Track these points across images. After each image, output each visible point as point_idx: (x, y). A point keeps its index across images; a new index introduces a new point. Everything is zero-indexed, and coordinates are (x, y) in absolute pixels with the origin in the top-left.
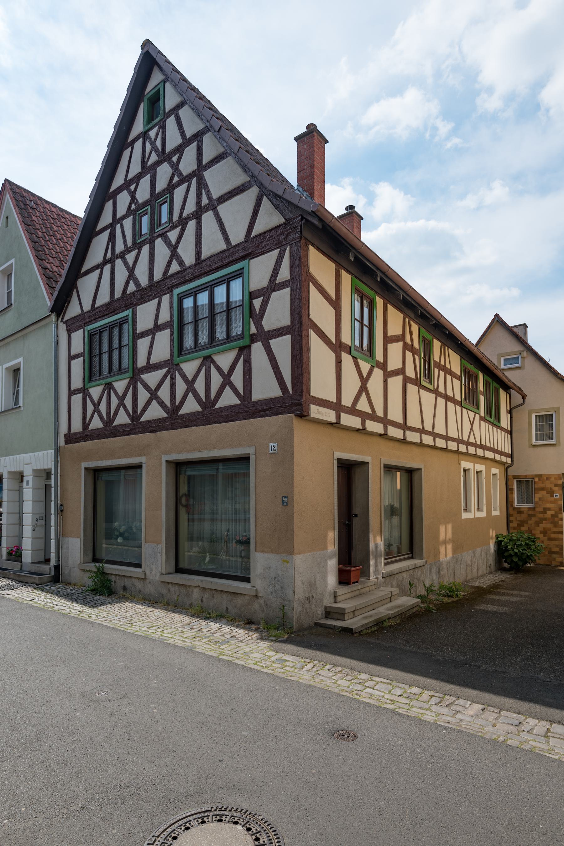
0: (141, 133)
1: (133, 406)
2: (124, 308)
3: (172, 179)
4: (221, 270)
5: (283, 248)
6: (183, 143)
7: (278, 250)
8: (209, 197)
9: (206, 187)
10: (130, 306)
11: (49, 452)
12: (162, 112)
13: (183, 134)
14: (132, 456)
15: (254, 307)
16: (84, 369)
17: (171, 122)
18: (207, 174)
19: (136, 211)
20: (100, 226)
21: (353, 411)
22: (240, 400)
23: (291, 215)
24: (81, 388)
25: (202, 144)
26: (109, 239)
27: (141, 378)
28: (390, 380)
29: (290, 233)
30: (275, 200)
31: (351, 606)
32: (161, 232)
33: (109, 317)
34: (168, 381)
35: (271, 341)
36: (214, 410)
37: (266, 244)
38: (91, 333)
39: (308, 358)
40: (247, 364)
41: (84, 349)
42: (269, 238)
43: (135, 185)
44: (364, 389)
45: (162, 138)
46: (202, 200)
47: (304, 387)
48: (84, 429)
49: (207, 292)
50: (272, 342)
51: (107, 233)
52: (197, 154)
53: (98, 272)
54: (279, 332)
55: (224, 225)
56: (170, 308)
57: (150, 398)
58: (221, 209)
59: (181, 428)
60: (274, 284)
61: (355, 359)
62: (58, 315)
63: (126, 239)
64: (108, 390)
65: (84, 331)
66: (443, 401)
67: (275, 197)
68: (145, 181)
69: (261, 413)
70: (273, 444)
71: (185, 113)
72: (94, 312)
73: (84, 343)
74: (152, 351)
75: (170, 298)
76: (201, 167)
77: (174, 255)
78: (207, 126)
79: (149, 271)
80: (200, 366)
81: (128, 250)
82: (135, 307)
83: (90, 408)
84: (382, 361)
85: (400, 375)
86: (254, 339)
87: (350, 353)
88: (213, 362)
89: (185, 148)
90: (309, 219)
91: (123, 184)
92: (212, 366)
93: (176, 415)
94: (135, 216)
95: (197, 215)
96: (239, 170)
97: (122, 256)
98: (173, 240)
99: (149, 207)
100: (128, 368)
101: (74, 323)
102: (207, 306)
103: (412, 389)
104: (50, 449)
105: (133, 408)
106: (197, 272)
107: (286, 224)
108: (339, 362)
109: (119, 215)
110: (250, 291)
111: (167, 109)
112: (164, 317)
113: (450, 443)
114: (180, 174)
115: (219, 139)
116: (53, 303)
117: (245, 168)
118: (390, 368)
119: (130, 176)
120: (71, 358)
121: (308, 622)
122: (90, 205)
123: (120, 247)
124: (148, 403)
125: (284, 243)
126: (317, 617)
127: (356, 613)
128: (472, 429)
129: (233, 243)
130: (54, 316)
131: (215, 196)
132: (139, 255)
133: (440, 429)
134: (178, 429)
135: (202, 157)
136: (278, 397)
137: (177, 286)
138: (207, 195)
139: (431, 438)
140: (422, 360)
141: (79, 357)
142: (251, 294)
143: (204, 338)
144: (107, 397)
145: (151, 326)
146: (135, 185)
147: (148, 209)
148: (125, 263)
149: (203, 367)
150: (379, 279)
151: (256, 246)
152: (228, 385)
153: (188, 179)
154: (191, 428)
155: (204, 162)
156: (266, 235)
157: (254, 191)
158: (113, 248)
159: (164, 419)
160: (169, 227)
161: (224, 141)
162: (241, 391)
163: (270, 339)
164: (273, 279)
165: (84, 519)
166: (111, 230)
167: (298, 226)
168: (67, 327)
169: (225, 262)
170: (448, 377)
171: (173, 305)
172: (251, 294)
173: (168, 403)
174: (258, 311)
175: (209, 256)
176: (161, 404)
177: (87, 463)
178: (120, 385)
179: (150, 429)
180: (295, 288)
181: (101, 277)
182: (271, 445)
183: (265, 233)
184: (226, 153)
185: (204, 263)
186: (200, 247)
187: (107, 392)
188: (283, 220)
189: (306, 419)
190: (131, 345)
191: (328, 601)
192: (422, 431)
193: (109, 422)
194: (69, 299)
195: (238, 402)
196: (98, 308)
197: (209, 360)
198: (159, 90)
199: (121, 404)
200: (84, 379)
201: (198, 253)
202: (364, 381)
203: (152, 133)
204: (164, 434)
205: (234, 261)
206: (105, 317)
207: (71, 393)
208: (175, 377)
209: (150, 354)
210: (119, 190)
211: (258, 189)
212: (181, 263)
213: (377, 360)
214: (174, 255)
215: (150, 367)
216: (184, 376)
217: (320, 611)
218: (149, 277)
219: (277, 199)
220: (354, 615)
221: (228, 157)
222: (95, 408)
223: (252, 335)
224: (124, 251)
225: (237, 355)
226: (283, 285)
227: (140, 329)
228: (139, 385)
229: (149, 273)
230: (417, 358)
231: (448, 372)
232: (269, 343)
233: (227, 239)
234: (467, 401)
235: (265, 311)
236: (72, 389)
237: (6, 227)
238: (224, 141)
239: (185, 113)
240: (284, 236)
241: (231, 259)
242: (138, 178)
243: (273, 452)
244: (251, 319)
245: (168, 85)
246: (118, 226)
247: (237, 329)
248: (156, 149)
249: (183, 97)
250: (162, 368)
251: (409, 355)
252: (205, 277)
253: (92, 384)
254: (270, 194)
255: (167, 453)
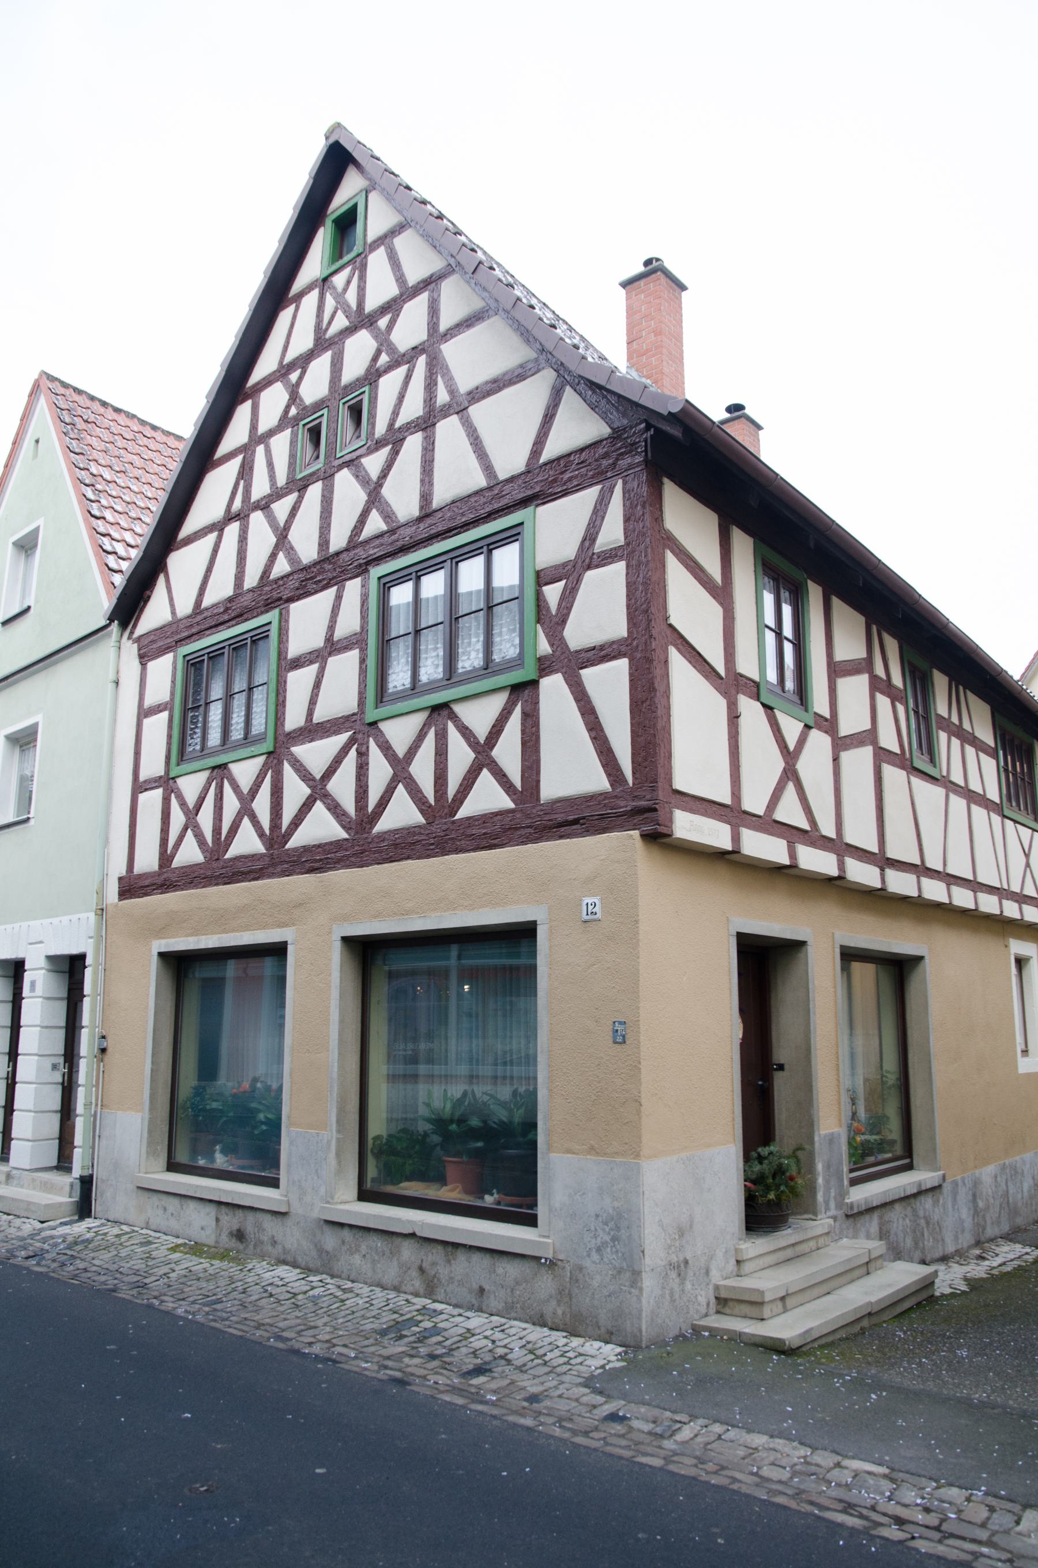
0: (317, 281)
1: (271, 814)
2: (263, 609)
3: (375, 358)
4: (474, 527)
5: (607, 484)
6: (402, 295)
7: (598, 487)
8: (452, 391)
9: (445, 371)
10: (277, 604)
11: (83, 916)
12: (362, 243)
13: (401, 279)
14: (264, 927)
15: (545, 601)
16: (170, 737)
17: (378, 260)
18: (448, 350)
19: (297, 420)
20: (223, 449)
21: (768, 824)
22: (513, 801)
23: (625, 422)
24: (161, 777)
25: (439, 295)
26: (239, 472)
27: (292, 754)
28: (845, 756)
29: (622, 454)
30: (590, 393)
31: (776, 1284)
32: (347, 458)
33: (229, 627)
34: (350, 761)
35: (583, 672)
36: (454, 822)
37: (572, 477)
38: (188, 661)
39: (668, 708)
40: (530, 722)
41: (172, 694)
42: (578, 464)
43: (299, 371)
44: (790, 774)
45: (359, 287)
46: (436, 396)
47: (661, 770)
48: (161, 866)
49: (441, 573)
50: (587, 674)
51: (236, 463)
52: (429, 314)
53: (212, 537)
54: (602, 654)
55: (481, 442)
56: (362, 605)
57: (310, 796)
58: (476, 411)
59: (379, 864)
60: (590, 554)
61: (768, 708)
62: (124, 625)
63: (274, 473)
64: (219, 779)
65: (175, 657)
66: (963, 802)
67: (590, 388)
68: (321, 365)
69: (563, 829)
70: (590, 900)
71: (406, 244)
72: (199, 618)
73: (173, 682)
74: (317, 695)
75: (363, 586)
76: (437, 336)
77: (375, 498)
78: (450, 265)
79: (320, 533)
80: (424, 725)
81: (277, 494)
82: (286, 605)
83: (178, 818)
84: (827, 714)
85: (866, 745)
86: (545, 666)
87: (758, 698)
88: (454, 717)
89: (405, 303)
90: (664, 428)
91: (275, 372)
92: (450, 726)
93: (366, 835)
94: (296, 428)
95: (426, 424)
96: (515, 340)
97: (264, 505)
98: (374, 472)
99: (325, 411)
100: (265, 733)
101: (153, 642)
102: (441, 604)
103: (893, 775)
104: (87, 911)
105: (272, 820)
106: (423, 530)
107: (614, 438)
108: (734, 718)
109: (262, 429)
110: (537, 568)
111: (371, 237)
112: (349, 623)
113: (983, 897)
114: (392, 349)
115: (473, 285)
116: (114, 601)
117: (526, 335)
118: (845, 729)
119: (290, 357)
120: (144, 713)
121: (674, 1324)
122: (206, 411)
123: (260, 488)
124: (307, 807)
125: (609, 474)
126: (697, 1311)
127: (790, 1302)
128: (1028, 865)
129: (502, 475)
130: (115, 626)
131: (464, 385)
132: (301, 502)
133: (960, 867)
134: (371, 865)
135: (438, 318)
136: (601, 794)
137: (378, 560)
138: (446, 387)
139: (942, 886)
140: (912, 713)
141: (161, 711)
142: (538, 574)
143: (431, 669)
144: (216, 795)
145: (318, 642)
146: (299, 371)
147: (323, 415)
148: (271, 520)
149: (430, 728)
150: (812, 544)
151: (550, 479)
152: (487, 766)
153: (408, 358)
154: (401, 863)
155: (443, 327)
156: (572, 458)
157: (545, 379)
158: (247, 491)
159: (338, 844)
160: (365, 447)
161: (485, 289)
162: (517, 780)
163: (582, 668)
164: (587, 543)
165: (152, 1070)
166: (244, 457)
167: (639, 442)
168: (139, 649)
169: (482, 512)
170: (970, 751)
171: (367, 599)
172: (538, 574)
173: (349, 805)
174: (554, 611)
175: (449, 501)
176: (335, 808)
177: (163, 942)
178: (245, 771)
179: (308, 865)
180: (634, 562)
181: (219, 547)
182: (585, 903)
183: (569, 455)
184: (487, 311)
185: (439, 515)
186: (431, 484)
187: (217, 784)
188: (606, 431)
189: (664, 843)
190: (273, 685)
191: (721, 1275)
192: (922, 870)
193: (217, 851)
194: (148, 592)
195: (507, 803)
196: (207, 609)
197: (445, 713)
198: (355, 206)
199: (246, 810)
200: (168, 758)
201: (426, 497)
202: (790, 756)
203: (339, 280)
204: (341, 877)
205: (503, 510)
206: (221, 628)
207: (139, 787)
208: (368, 751)
209: (313, 702)
210: (267, 382)
211: (554, 374)
212: (388, 515)
213: (815, 713)
214: (375, 498)
215: (312, 731)
216: (386, 748)
217: (704, 1297)
218: (319, 545)
219: (594, 392)
220: (784, 1306)
221: (492, 316)
222: (188, 819)
223: (540, 660)
224: (269, 495)
225: (507, 702)
226: (609, 557)
227: (294, 650)
228: (287, 769)
229: (320, 537)
230: (900, 709)
231: (969, 739)
232: (579, 676)
233: (488, 468)
234: (1014, 804)
235: (569, 609)
236: (142, 778)
237: (33, 459)
238: (485, 289)
239: (406, 244)
240: (611, 461)
241: (496, 506)
242: (304, 361)
243: (590, 917)
244: (538, 626)
245: (373, 197)
246: (260, 450)
247: (506, 647)
248: (345, 306)
249: (403, 216)
250: (337, 732)
251: (883, 702)
252: (439, 541)
253: (185, 767)
254: (579, 382)
255: (345, 918)
